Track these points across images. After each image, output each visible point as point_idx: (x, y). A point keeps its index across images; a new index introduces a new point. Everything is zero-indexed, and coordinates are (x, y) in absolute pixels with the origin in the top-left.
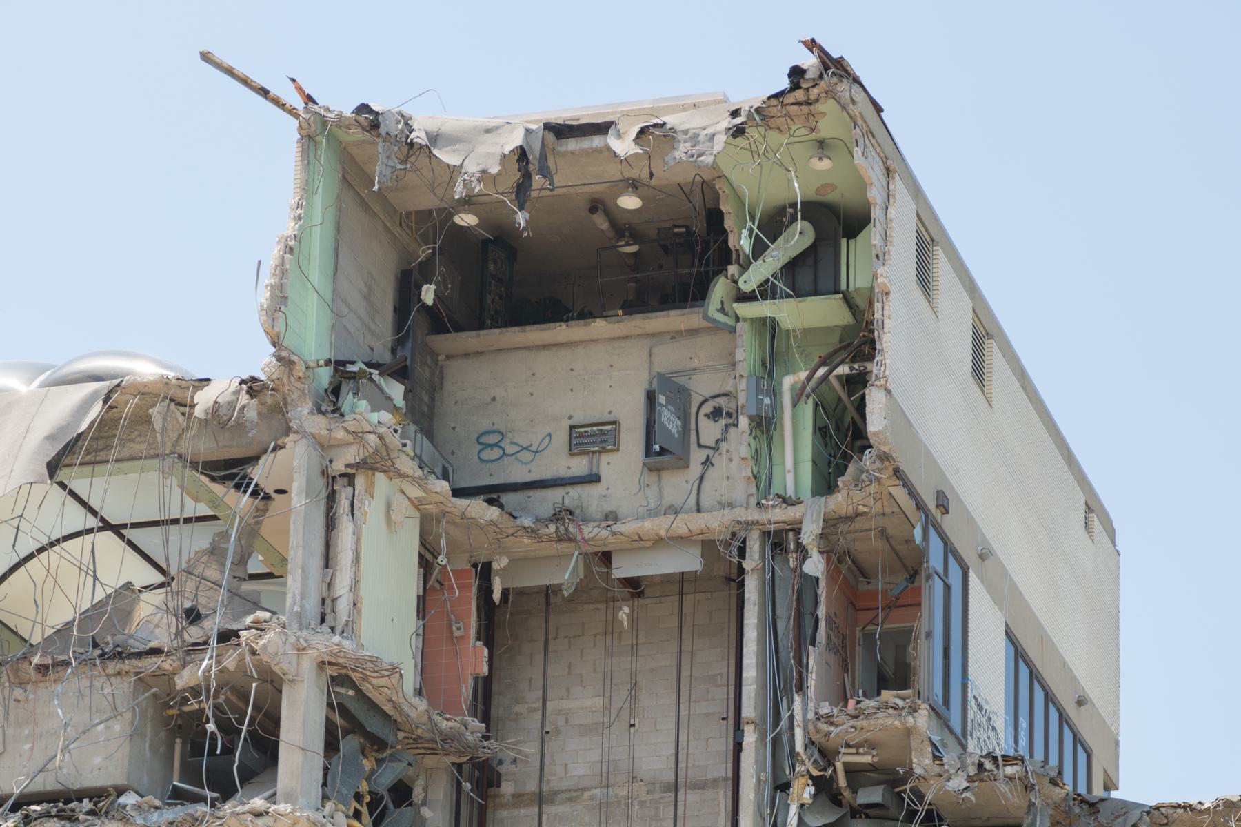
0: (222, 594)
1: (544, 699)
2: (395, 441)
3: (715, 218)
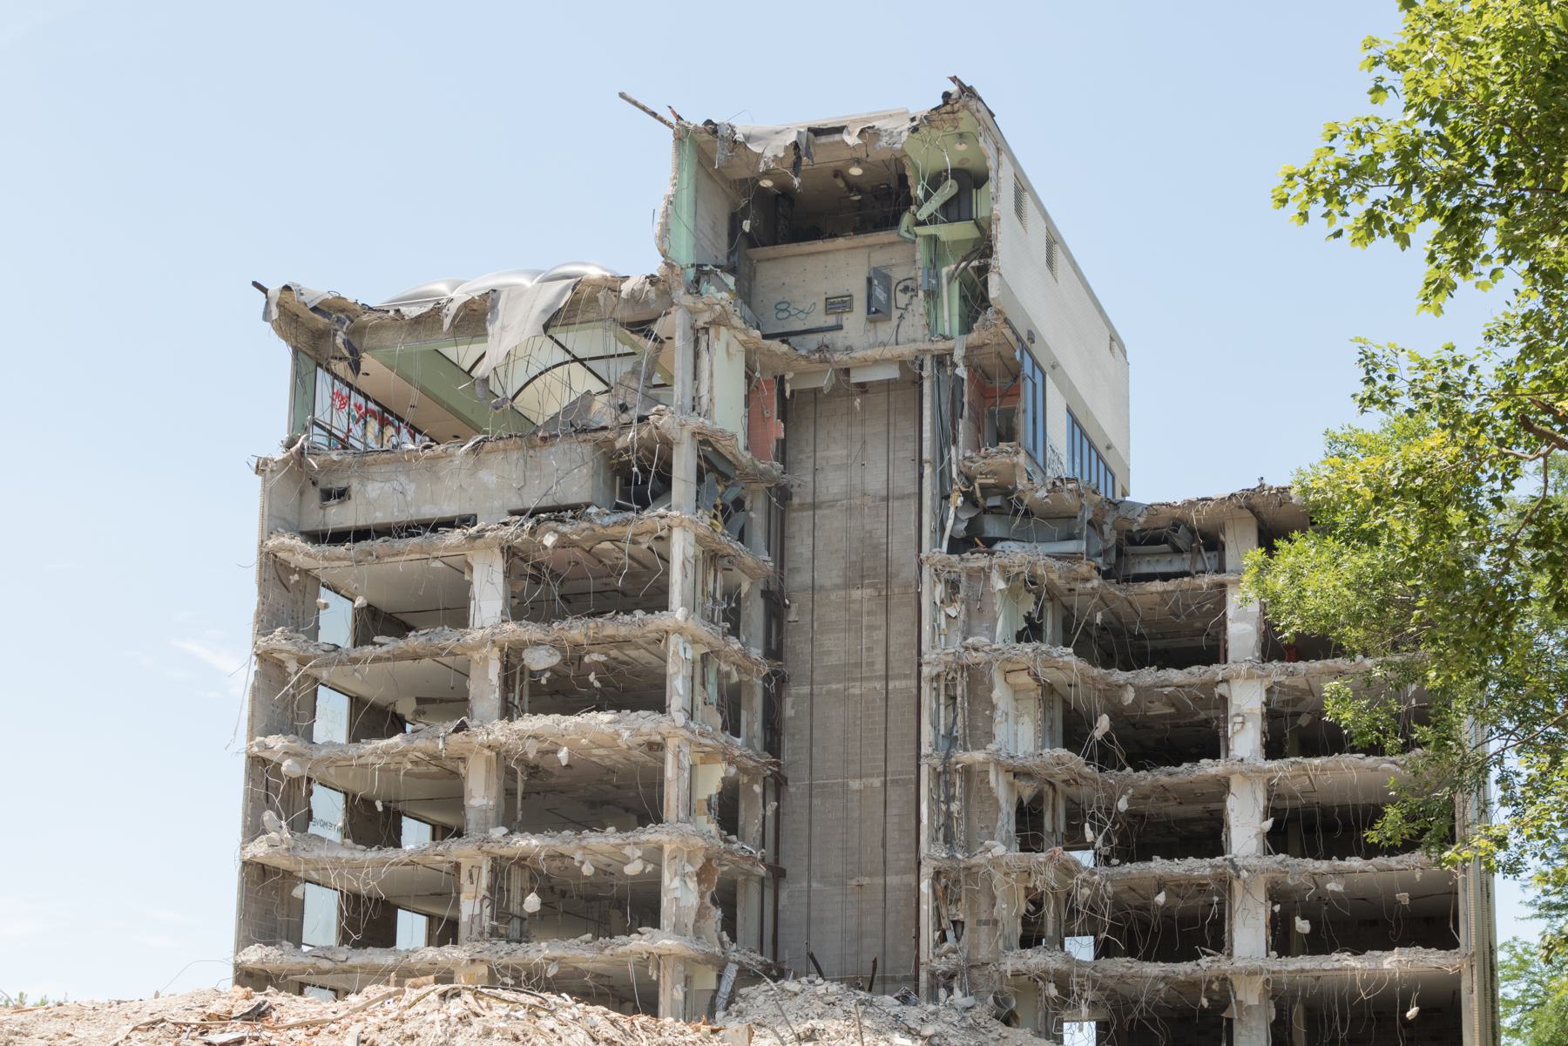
1: (815, 451)
2: (730, 308)
3: (903, 179)
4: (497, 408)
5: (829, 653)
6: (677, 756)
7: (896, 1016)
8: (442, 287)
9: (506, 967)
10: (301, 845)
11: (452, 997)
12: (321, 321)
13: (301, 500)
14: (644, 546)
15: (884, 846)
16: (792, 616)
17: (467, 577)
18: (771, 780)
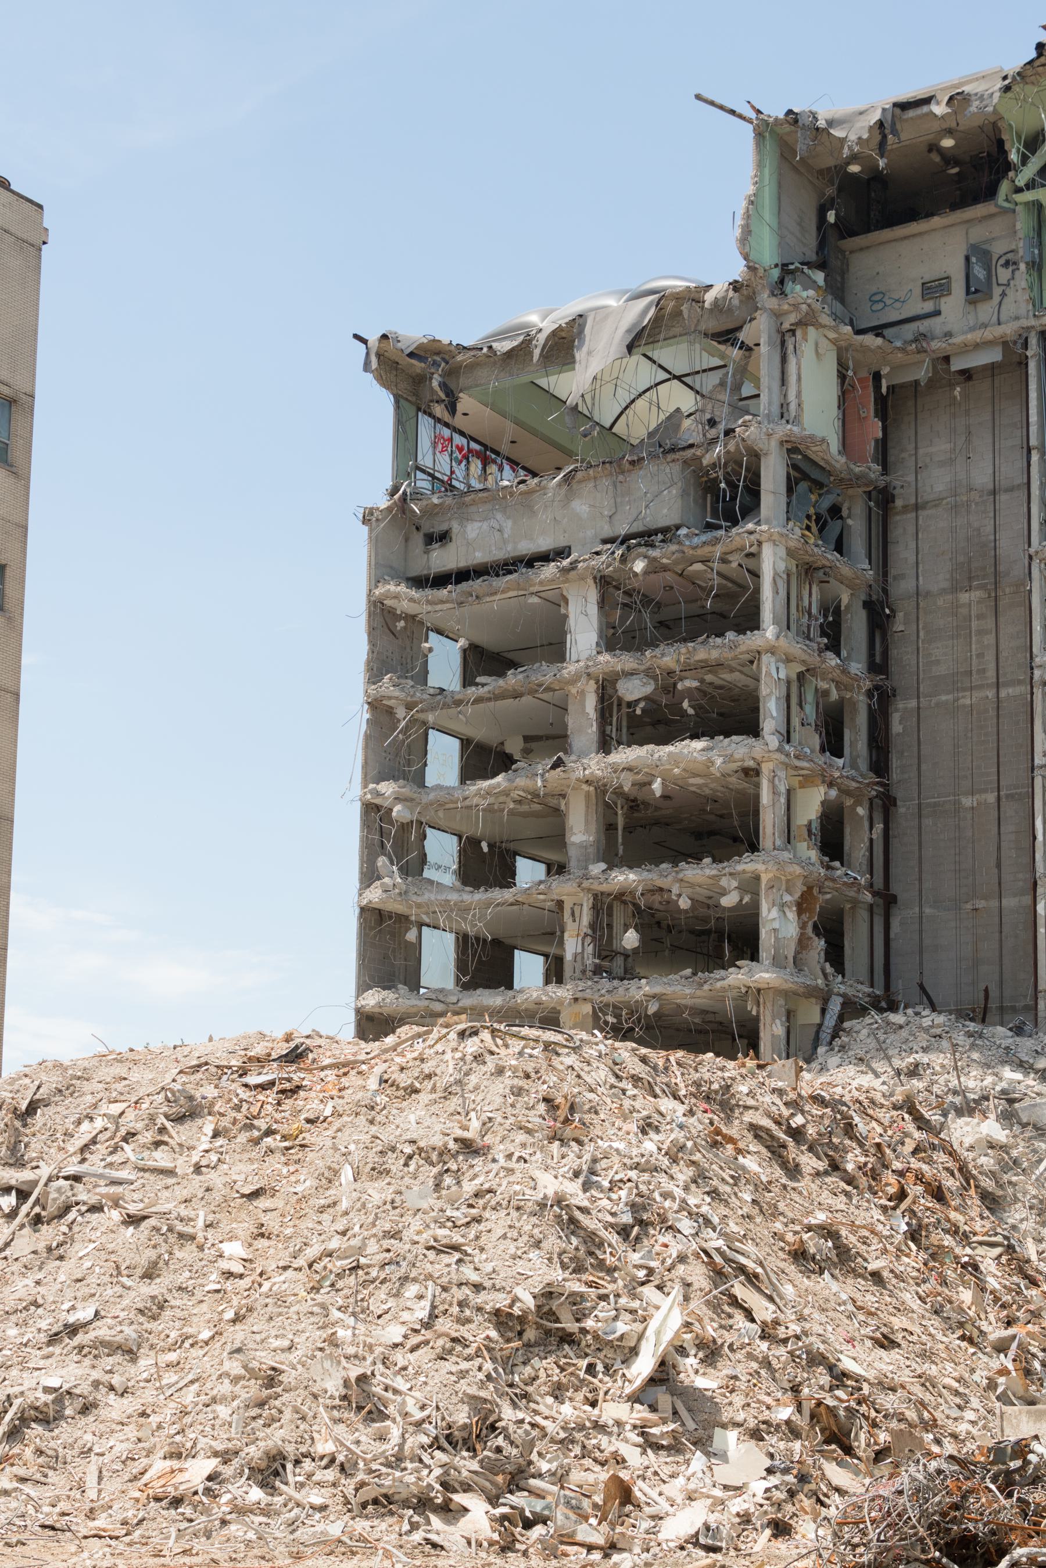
0: (726, 409)
1: (916, 448)
2: (818, 306)
3: (1001, 143)
4: (585, 436)
5: (938, 662)
6: (772, 781)
7: (1007, 1048)
8: (534, 318)
9: (607, 1005)
10: (413, 889)
11: (470, 1036)
12: (418, 365)
13: (406, 547)
14: (734, 565)
15: (999, 866)
16: (898, 626)
17: (563, 611)
18: (878, 802)
